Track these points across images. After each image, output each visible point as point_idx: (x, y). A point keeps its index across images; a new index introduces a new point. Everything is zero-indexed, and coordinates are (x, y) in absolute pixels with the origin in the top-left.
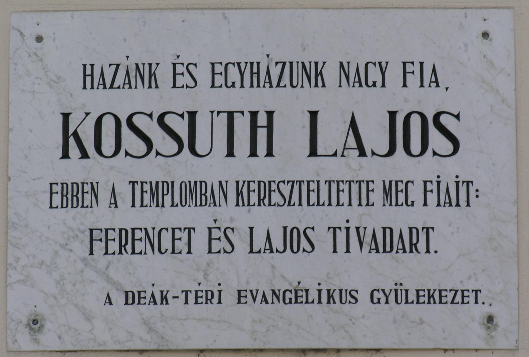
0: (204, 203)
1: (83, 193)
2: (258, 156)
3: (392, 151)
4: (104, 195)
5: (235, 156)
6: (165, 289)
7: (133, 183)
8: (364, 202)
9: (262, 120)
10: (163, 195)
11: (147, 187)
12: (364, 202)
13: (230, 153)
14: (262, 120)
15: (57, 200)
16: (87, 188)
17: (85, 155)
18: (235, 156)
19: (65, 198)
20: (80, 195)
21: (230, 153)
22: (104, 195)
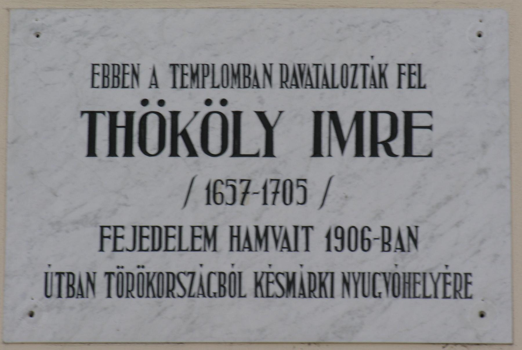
0: (116, 85)
1: (124, 74)
2: (274, 157)
3: (134, 249)
4: (145, 77)
5: (274, 156)
6: (383, 62)
7: (174, 66)
8: (178, 84)
9: (121, 120)
10: (204, 76)
11: (187, 70)
12: (178, 84)
13: (333, 65)
14: (121, 120)
15: (98, 81)
16: (128, 69)
17: (192, 153)
18: (274, 156)
19: (106, 79)
20: (121, 76)
21: (333, 65)
22: (145, 77)
